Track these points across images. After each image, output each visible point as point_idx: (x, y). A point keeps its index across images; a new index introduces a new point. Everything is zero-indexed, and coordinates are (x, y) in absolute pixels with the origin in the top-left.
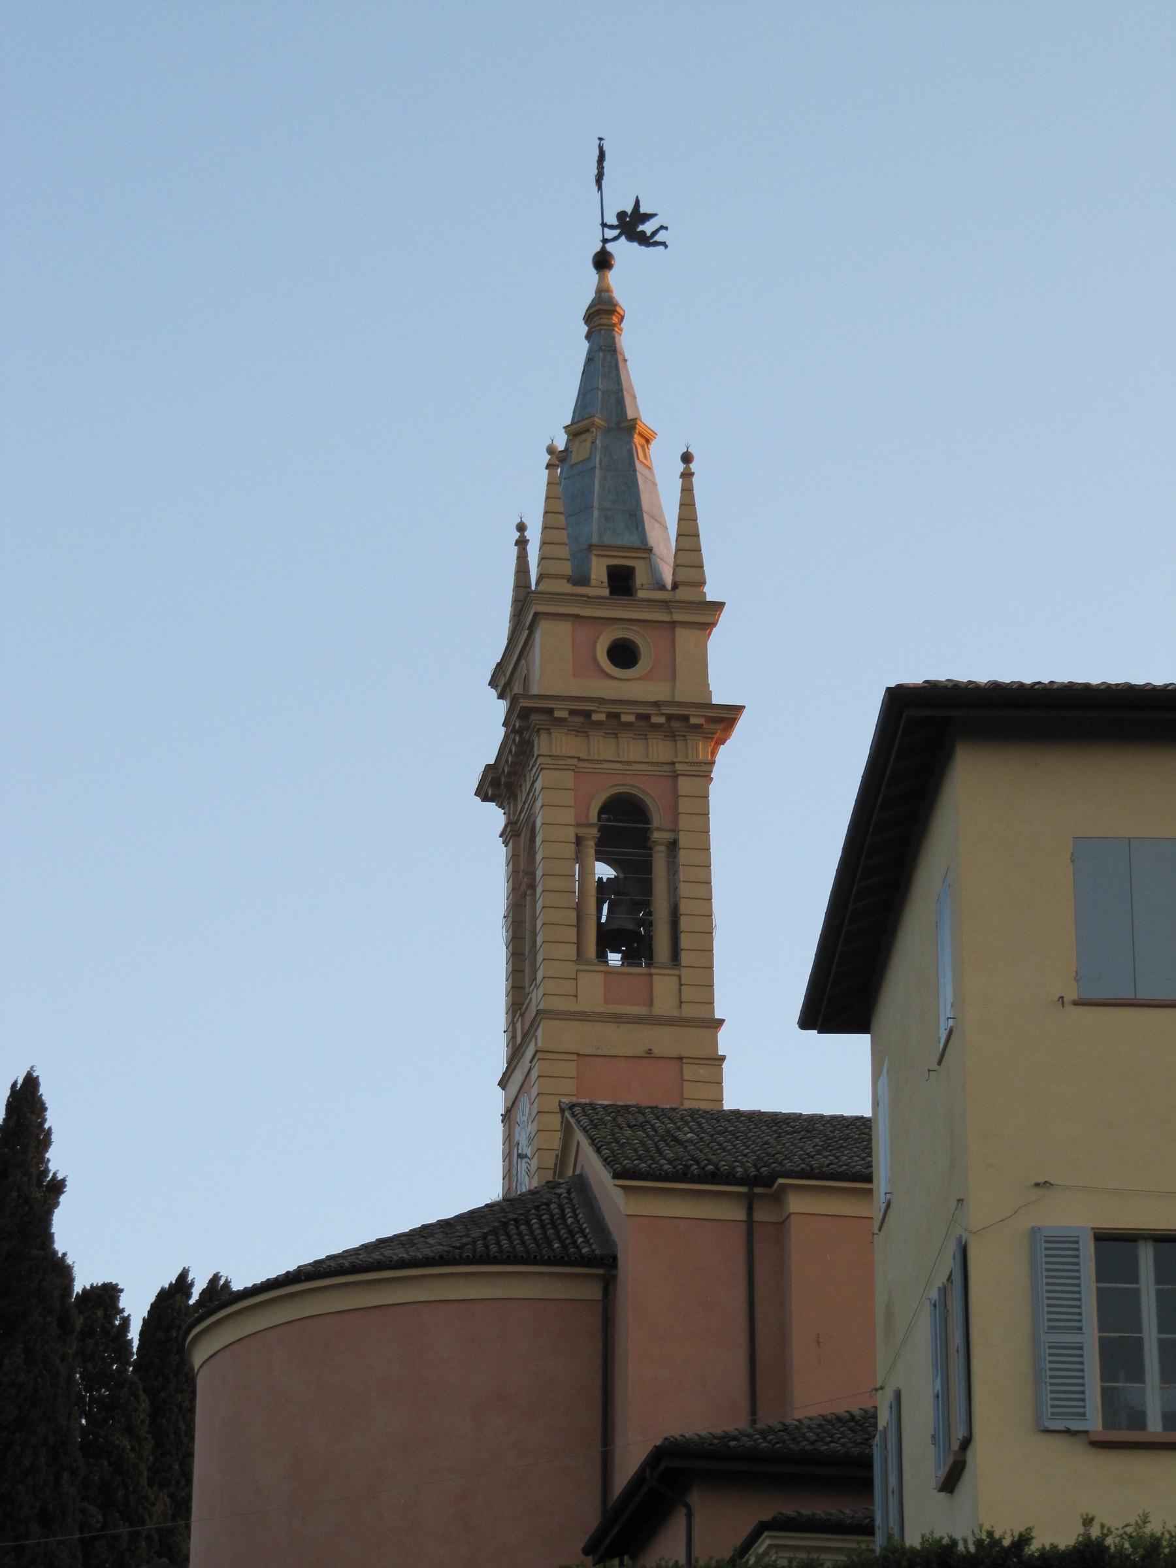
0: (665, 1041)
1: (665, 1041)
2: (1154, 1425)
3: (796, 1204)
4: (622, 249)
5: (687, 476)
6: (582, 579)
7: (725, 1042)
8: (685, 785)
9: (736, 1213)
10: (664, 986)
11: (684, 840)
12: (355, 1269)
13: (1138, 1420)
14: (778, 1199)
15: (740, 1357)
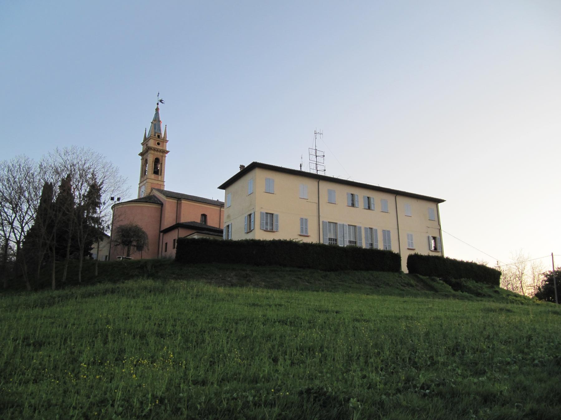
0: (160, 183)
1: (160, 183)
2: (269, 230)
3: (183, 201)
4: (160, 103)
5: (166, 127)
6: (155, 135)
7: (165, 183)
8: (163, 158)
9: (176, 201)
10: (160, 177)
11: (163, 163)
12: (136, 202)
13: (267, 229)
14: (181, 201)
15: (175, 215)
